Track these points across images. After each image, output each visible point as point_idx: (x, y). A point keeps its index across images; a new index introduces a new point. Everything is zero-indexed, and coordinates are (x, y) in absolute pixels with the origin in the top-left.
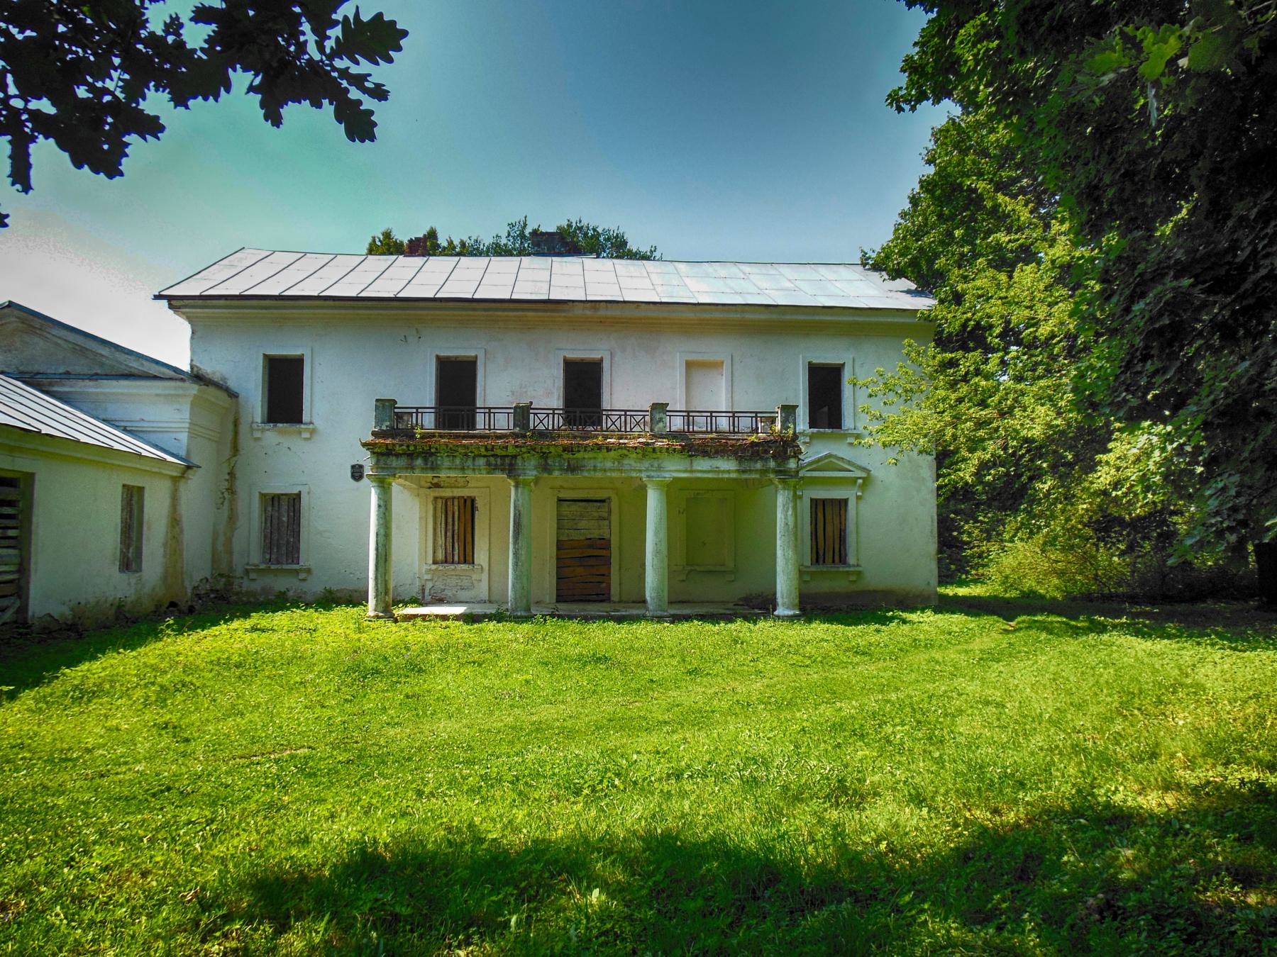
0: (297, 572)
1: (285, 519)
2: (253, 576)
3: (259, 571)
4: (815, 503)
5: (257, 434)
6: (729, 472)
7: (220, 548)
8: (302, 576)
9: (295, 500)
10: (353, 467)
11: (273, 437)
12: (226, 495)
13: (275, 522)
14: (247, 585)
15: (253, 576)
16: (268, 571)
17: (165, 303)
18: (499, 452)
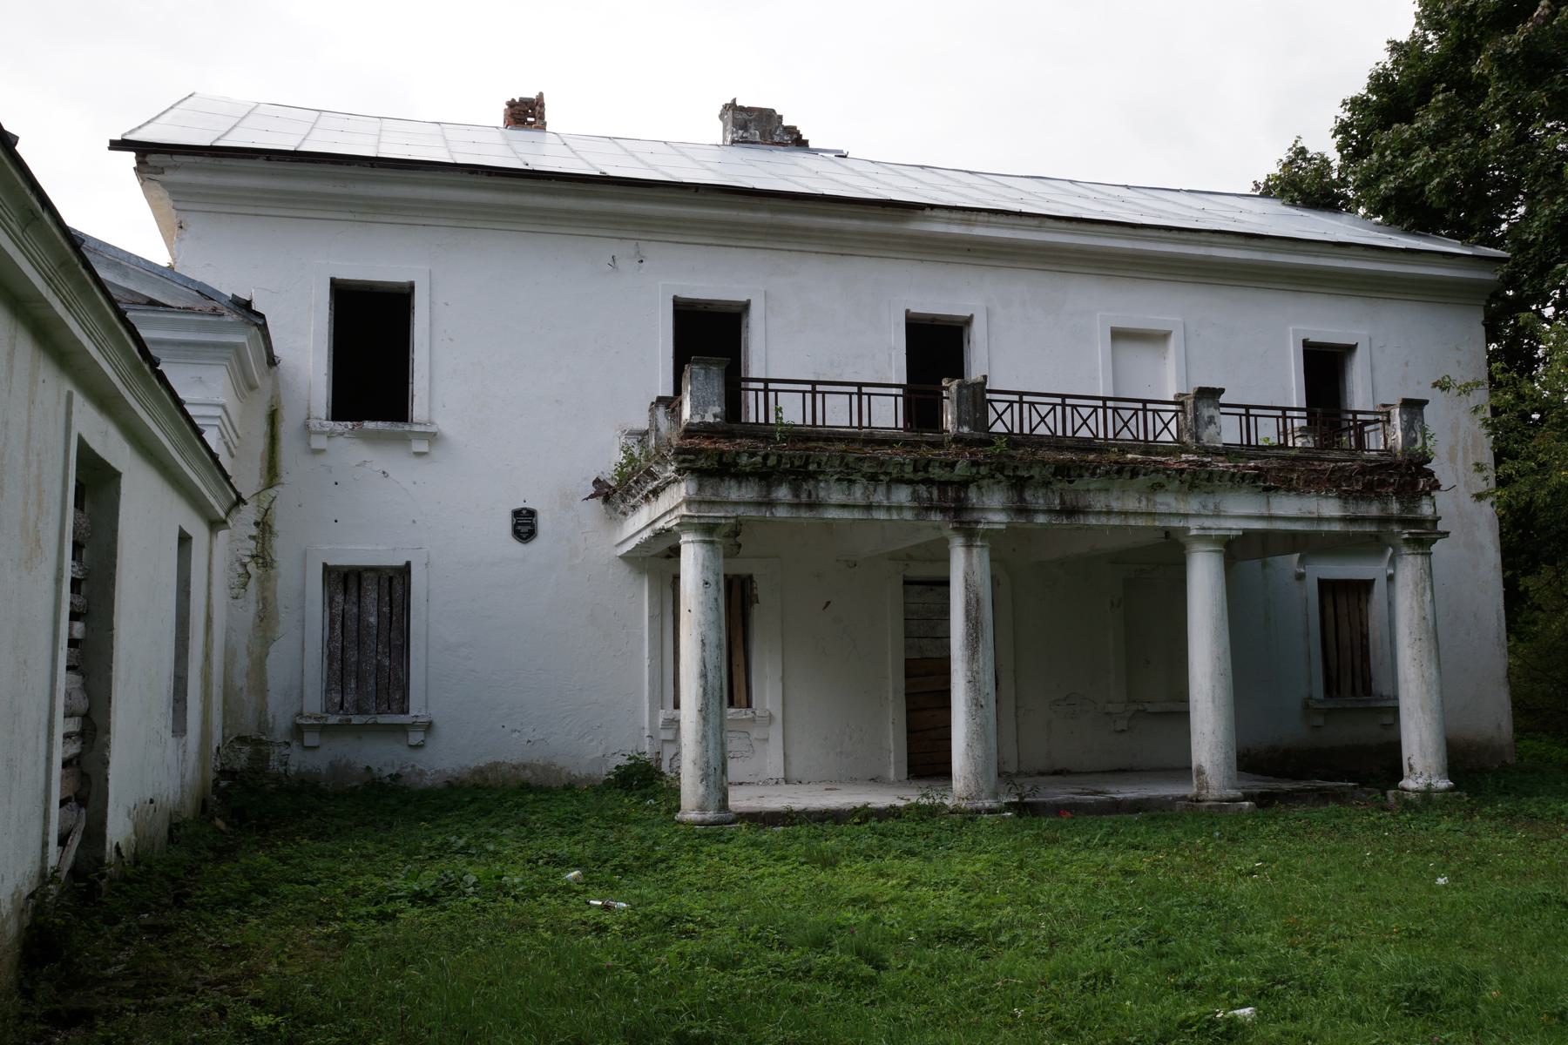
0: (403, 729)
1: (373, 620)
2: (311, 739)
3: (324, 729)
4: (1324, 585)
5: (318, 442)
6: (1330, 520)
7: (240, 681)
8: (416, 738)
9: (395, 581)
10: (517, 513)
11: (356, 454)
12: (252, 568)
13: (352, 625)
14: (299, 761)
15: (311, 739)
16: (344, 728)
17: (129, 158)
18: (936, 472)
